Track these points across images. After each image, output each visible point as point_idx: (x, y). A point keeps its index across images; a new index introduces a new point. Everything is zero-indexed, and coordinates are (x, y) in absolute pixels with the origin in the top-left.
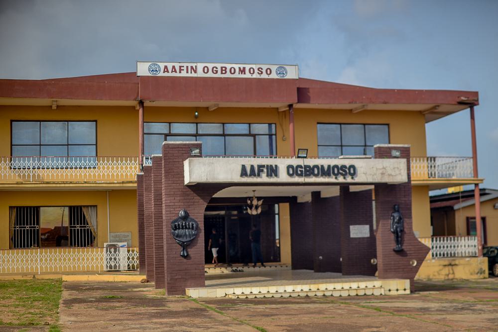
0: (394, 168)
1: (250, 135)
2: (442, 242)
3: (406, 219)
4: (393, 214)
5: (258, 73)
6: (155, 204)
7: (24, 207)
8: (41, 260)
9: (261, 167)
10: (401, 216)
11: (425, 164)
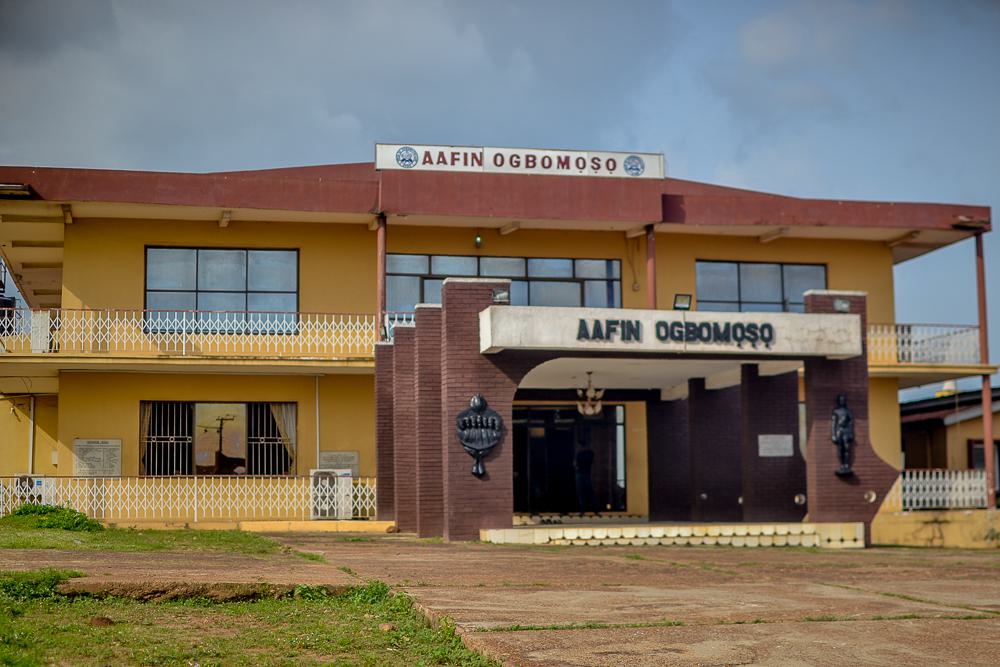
0: (839, 331)
1: (574, 279)
3: (858, 421)
5: (593, 167)
7: (166, 403)
8: (199, 497)
9: (611, 324)
10: (851, 416)
11: (892, 336)
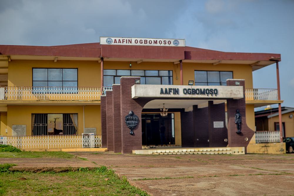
0: (237, 91)
1: (159, 76)
2: (261, 134)
3: (242, 117)
5: (164, 43)
8: (49, 141)
9: (170, 89)
10: (241, 116)
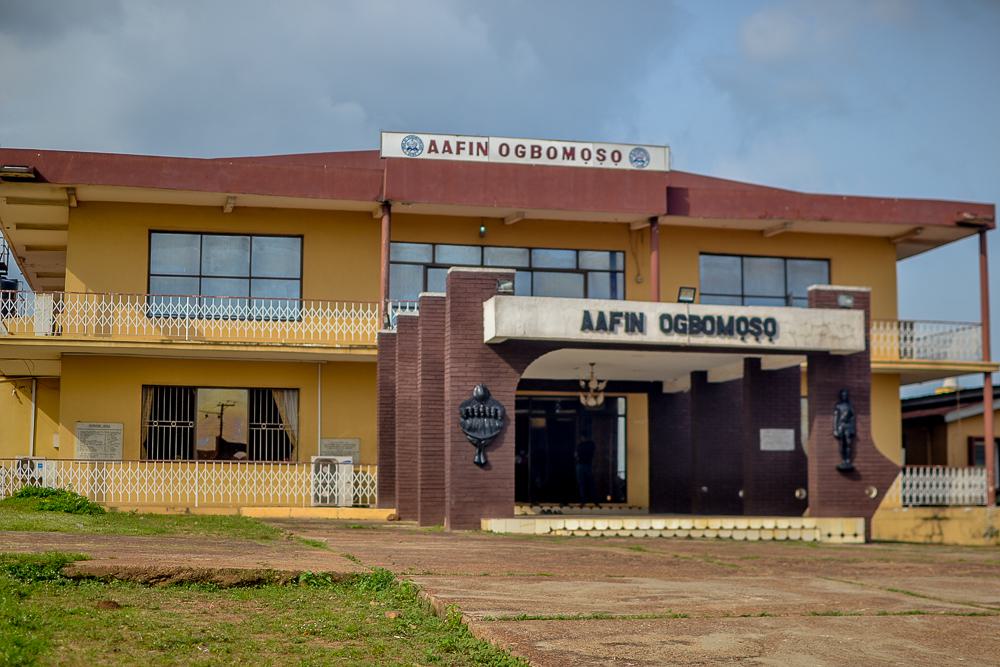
0: (843, 326)
1: (577, 270)
3: (859, 416)
4: (838, 406)
5: (598, 159)
6: (423, 379)
8: (200, 482)
9: (615, 316)
10: (853, 411)
11: (894, 332)
